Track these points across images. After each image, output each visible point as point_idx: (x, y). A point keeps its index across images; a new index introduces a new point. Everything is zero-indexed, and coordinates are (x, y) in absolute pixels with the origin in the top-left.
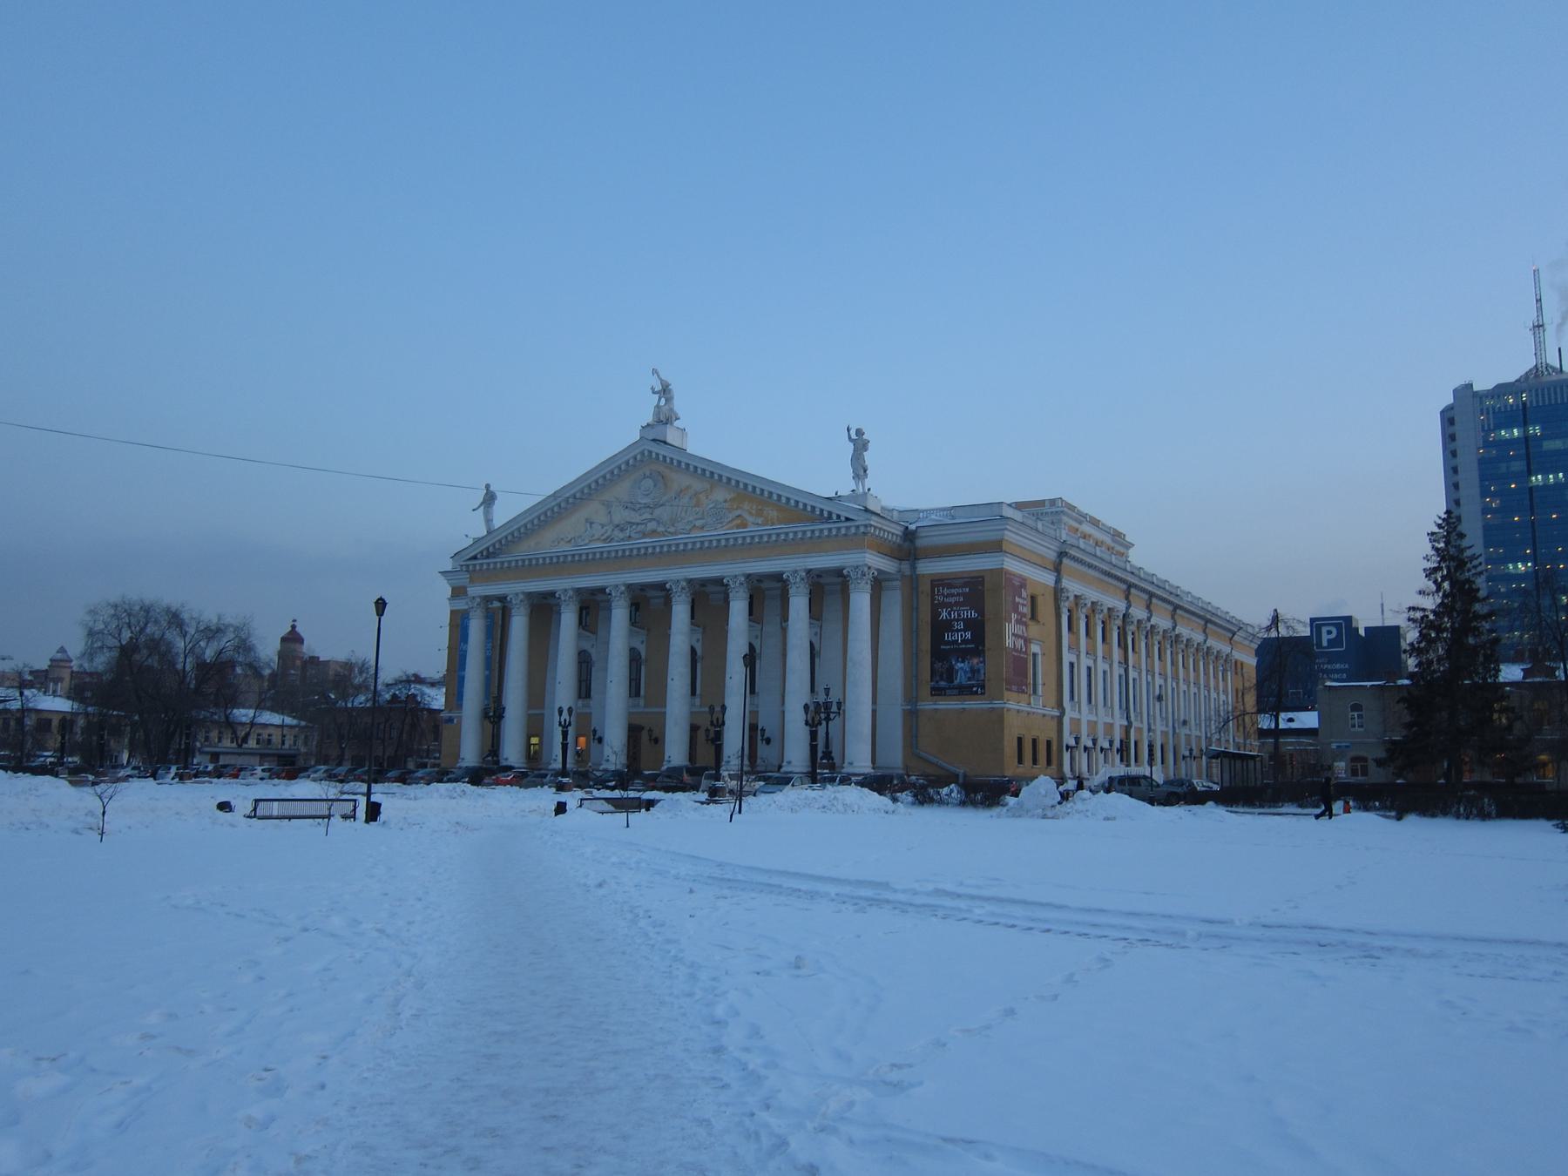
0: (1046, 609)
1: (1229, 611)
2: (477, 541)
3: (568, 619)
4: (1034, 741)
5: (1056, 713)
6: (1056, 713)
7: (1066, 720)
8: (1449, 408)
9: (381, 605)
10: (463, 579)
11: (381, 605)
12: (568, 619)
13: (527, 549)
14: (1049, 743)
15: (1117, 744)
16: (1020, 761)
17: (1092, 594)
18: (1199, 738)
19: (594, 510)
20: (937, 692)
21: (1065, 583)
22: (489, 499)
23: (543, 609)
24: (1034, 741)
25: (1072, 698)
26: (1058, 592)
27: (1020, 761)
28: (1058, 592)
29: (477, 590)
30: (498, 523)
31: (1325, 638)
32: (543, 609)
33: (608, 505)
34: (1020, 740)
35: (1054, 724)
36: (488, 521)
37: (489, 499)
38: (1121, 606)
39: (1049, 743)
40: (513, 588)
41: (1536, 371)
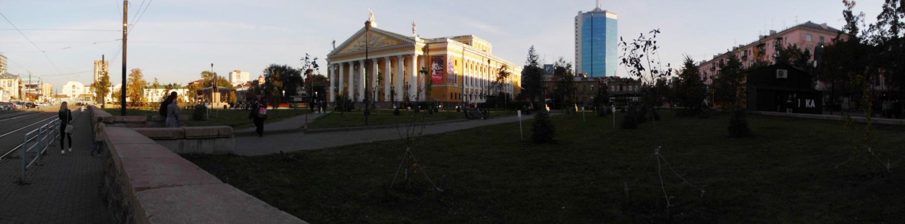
0: (459, 63)
1: (319, 65)
2: (332, 52)
3: (351, 68)
4: (456, 94)
5: (462, 87)
6: (462, 87)
7: (464, 89)
8: (576, 17)
9: (212, 65)
10: (329, 60)
11: (212, 65)
12: (351, 68)
13: (342, 52)
14: (460, 94)
15: (479, 94)
16: (452, 98)
17: (472, 59)
18: (477, 90)
19: (356, 43)
20: (872, 117)
21: (465, 57)
22: (334, 42)
23: (346, 65)
24: (456, 94)
25: (466, 84)
26: (463, 60)
27: (452, 98)
28: (463, 60)
29: (332, 63)
30: (336, 47)
31: (547, 69)
32: (346, 65)
33: (359, 42)
34: (452, 93)
35: (461, 90)
36: (334, 47)
37: (334, 42)
38: (481, 62)
39: (460, 94)
40: (340, 62)
41: (596, 9)
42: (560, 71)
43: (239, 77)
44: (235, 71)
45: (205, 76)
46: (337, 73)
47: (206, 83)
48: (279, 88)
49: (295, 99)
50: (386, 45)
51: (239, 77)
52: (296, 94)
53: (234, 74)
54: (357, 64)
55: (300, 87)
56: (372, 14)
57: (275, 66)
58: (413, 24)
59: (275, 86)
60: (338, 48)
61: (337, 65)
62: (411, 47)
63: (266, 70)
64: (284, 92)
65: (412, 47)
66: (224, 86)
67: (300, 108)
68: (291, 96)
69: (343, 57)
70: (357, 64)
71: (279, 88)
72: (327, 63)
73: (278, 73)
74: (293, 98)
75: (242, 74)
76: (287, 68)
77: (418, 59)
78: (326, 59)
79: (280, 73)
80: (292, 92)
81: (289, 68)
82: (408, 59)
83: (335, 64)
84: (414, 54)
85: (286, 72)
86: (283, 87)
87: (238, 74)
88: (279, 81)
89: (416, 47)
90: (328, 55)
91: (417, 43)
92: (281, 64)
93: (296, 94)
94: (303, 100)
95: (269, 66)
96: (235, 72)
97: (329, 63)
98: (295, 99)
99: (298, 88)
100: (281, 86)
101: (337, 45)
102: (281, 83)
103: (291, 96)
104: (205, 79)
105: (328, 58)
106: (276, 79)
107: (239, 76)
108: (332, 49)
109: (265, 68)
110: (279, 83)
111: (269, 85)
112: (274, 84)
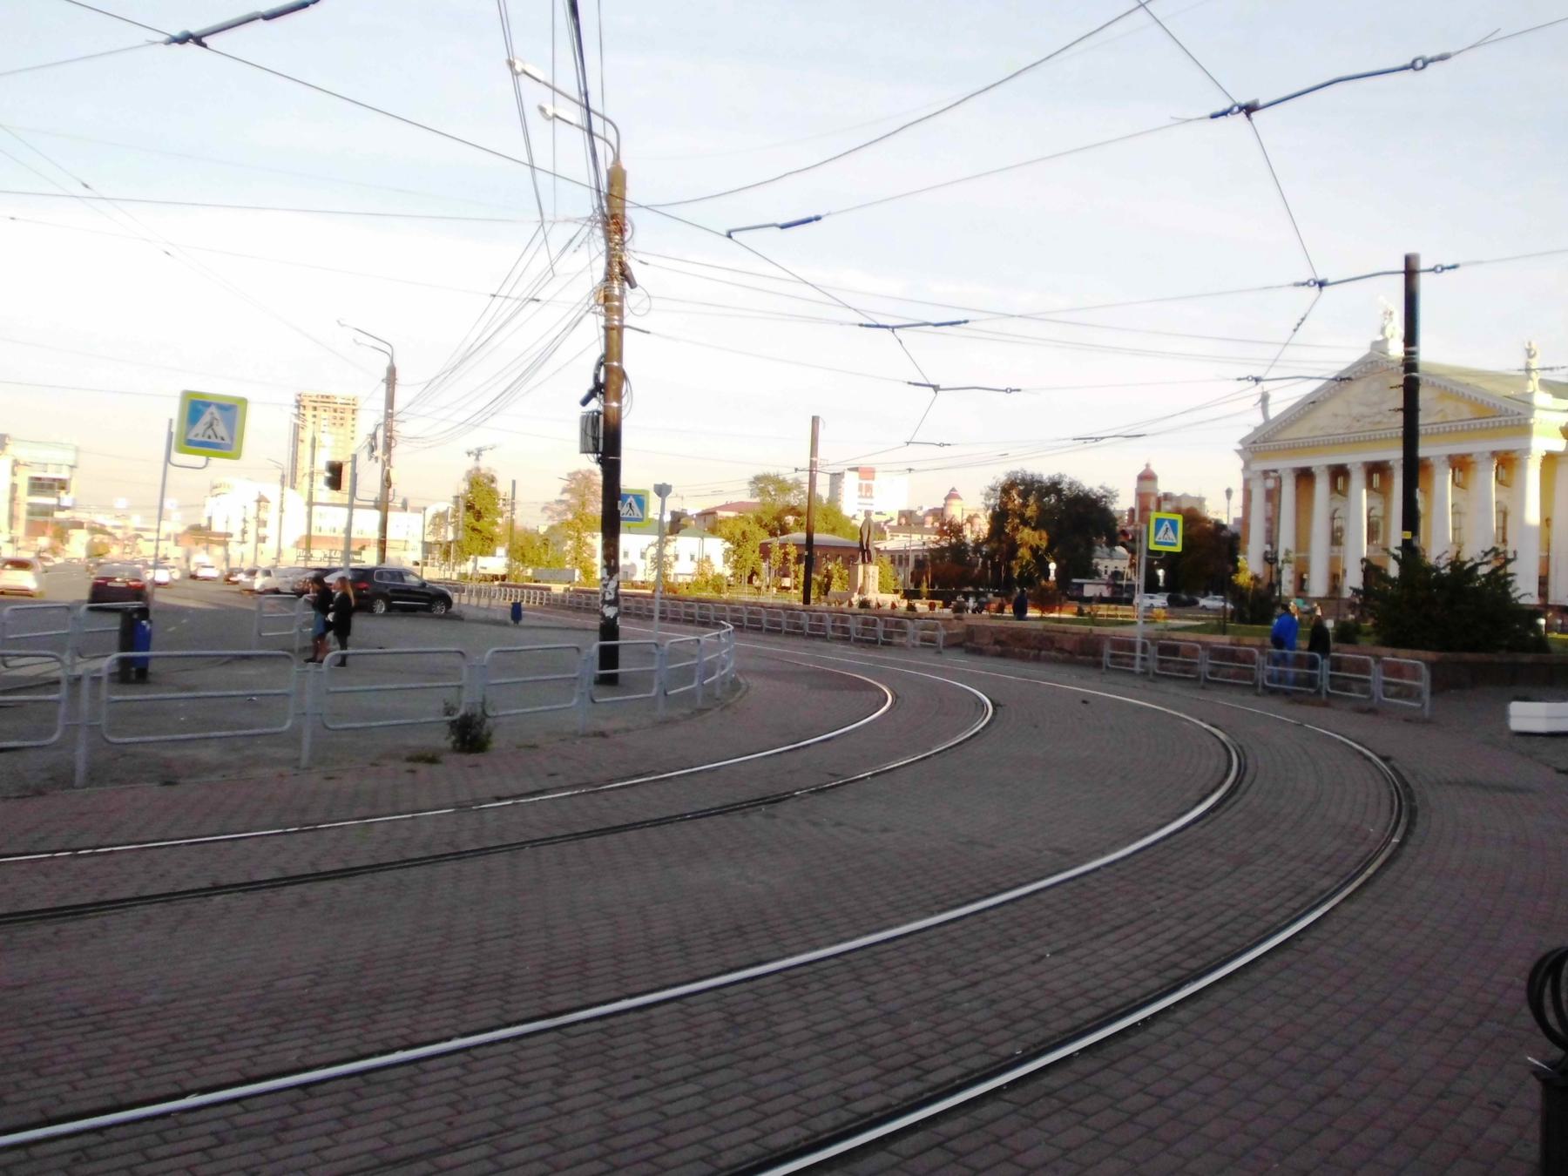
2: (1257, 429)
3: (1322, 486)
10: (1249, 455)
12: (1322, 486)
23: (1305, 477)
32: (1305, 477)
42: (1219, 527)
43: (866, 491)
44: (856, 469)
45: (763, 492)
46: (1273, 496)
47: (767, 519)
48: (1034, 550)
49: (1090, 590)
50: (1437, 419)
51: (866, 491)
52: (1091, 573)
53: (851, 482)
54: (1339, 473)
55: (1106, 550)
56: (1391, 313)
57: (1023, 481)
58: (1529, 351)
59: (1020, 546)
60: (1277, 418)
61: (1272, 474)
62: (1518, 425)
63: (994, 490)
64: (1053, 566)
65: (1523, 428)
66: (833, 531)
67: (1101, 616)
68: (1075, 581)
69: (1293, 449)
70: (1339, 473)
71: (1034, 550)
72: (1240, 463)
73: (1031, 500)
74: (1081, 586)
75: (880, 482)
76: (1064, 486)
77: (1542, 465)
78: (1238, 452)
79: (1039, 500)
80: (1079, 567)
81: (1071, 484)
82: (1508, 463)
83: (1266, 474)
84: (1527, 451)
85: (1059, 500)
86: (1049, 549)
87: (864, 482)
88: (1034, 529)
89: (1535, 428)
90: (1242, 442)
91: (1537, 414)
92: (1044, 468)
93: (1091, 573)
94: (1114, 593)
95: (1002, 478)
96: (855, 474)
97: (1246, 467)
98: (1090, 590)
99: (1101, 550)
100: (1044, 544)
101: (1274, 411)
102: (1044, 535)
103: (1075, 581)
104: (763, 504)
105: (1245, 449)
106: (1025, 522)
107: (869, 488)
108: (1258, 420)
109: (991, 482)
110: (1037, 535)
111: (1000, 541)
112: (1018, 537)
